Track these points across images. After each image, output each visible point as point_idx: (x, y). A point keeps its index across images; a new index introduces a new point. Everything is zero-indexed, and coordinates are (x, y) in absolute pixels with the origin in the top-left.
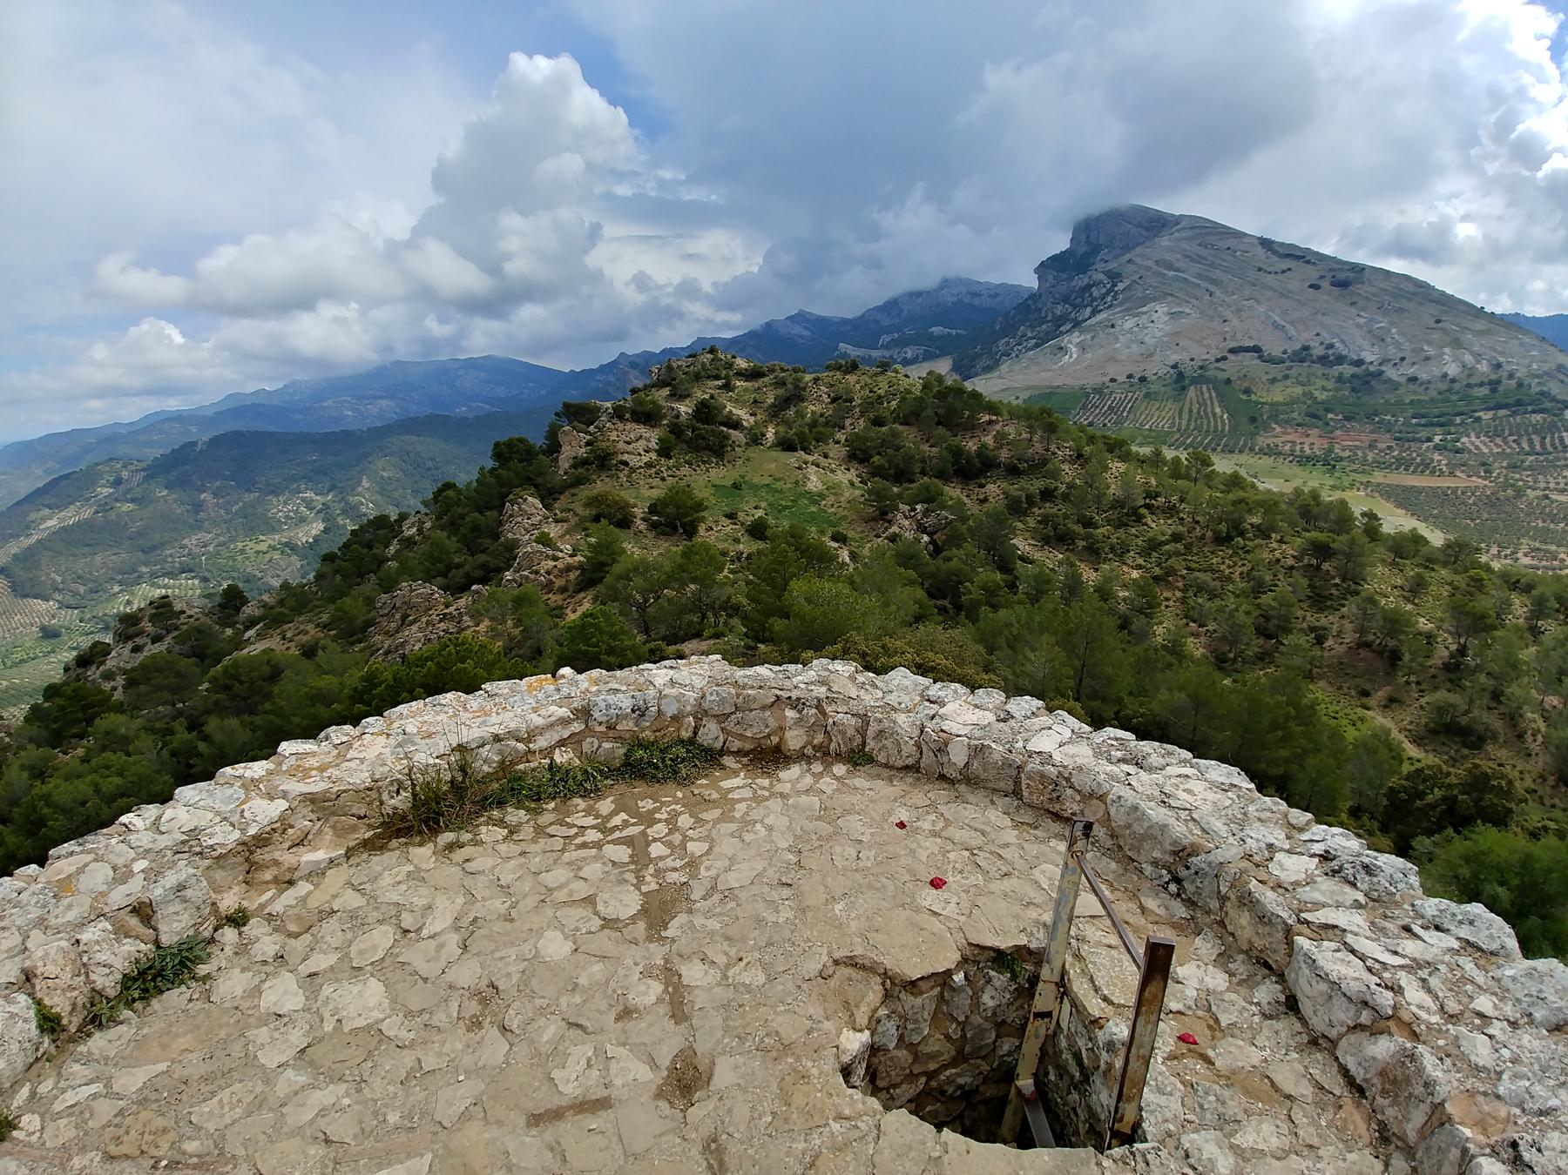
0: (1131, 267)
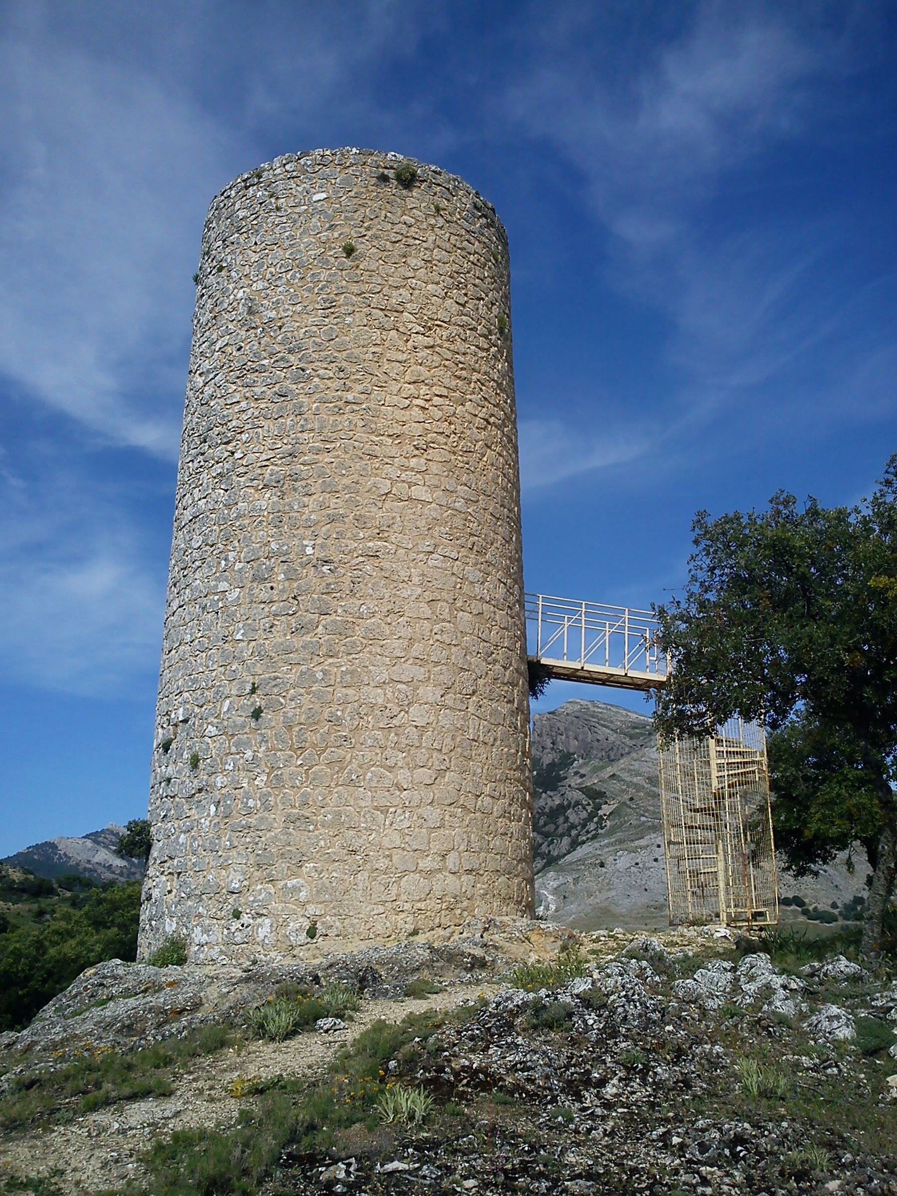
0: (616, 786)
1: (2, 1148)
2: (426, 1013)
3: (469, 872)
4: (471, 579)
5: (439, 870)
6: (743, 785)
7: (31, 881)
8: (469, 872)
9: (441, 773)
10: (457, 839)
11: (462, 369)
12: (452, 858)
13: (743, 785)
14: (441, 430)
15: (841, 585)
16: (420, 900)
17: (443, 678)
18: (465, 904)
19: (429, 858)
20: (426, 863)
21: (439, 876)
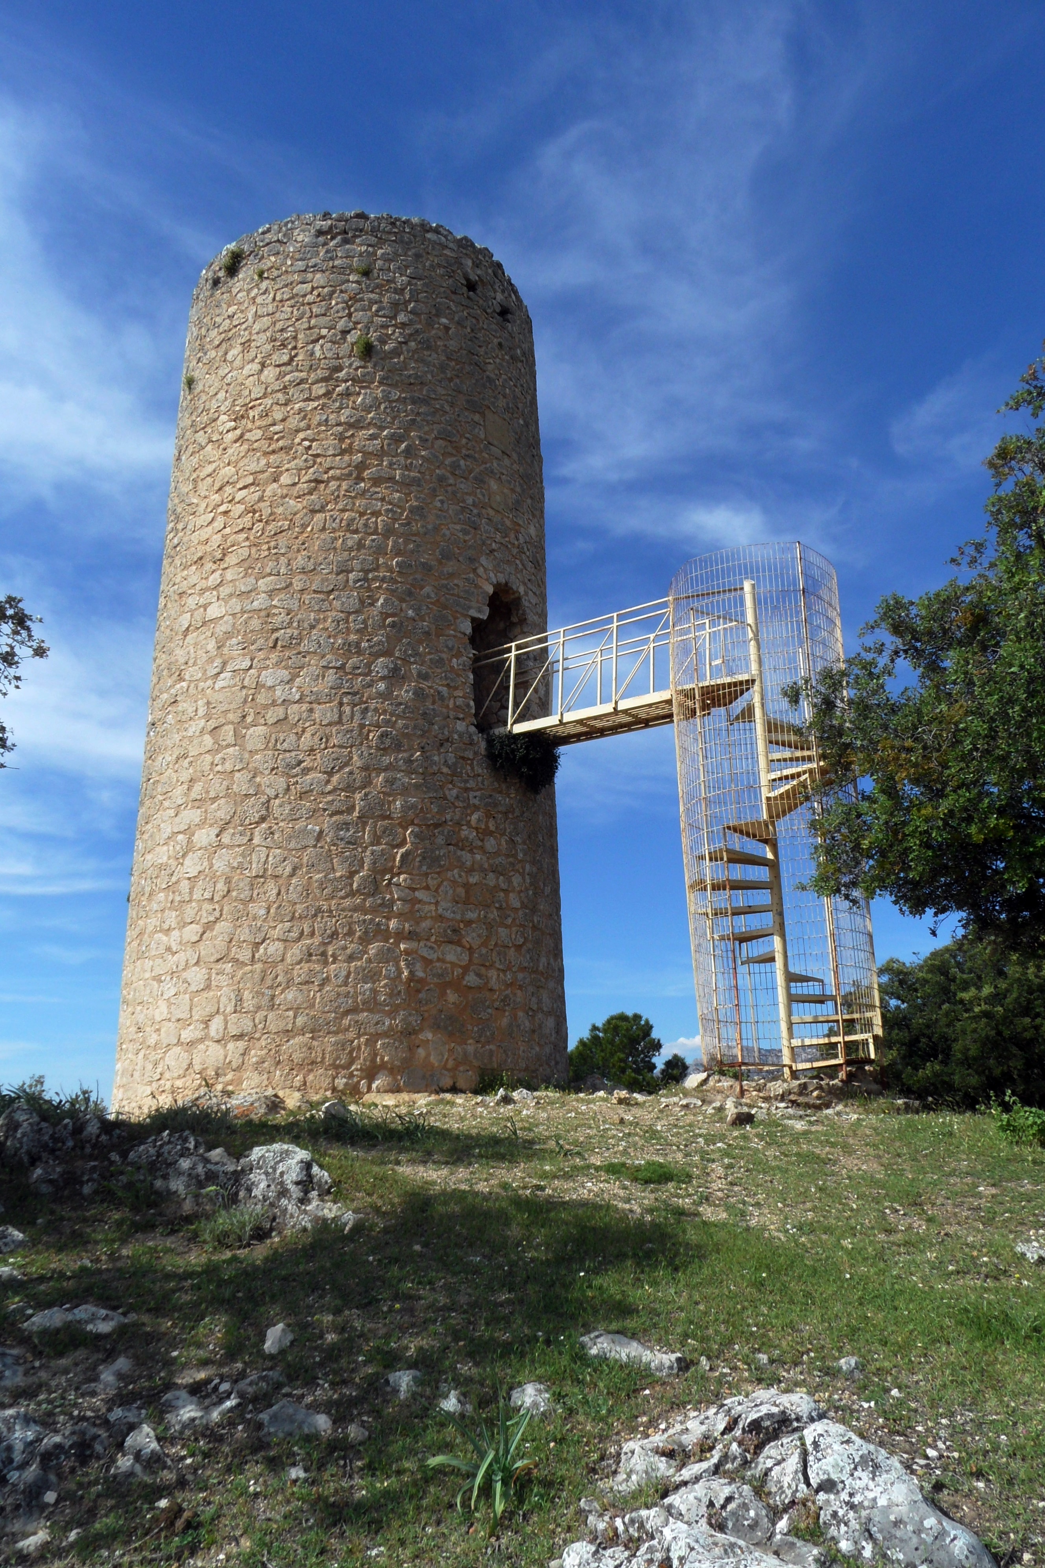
1: (4, 1270)
2: (879, 1094)
3: (240, 1037)
4: (269, 684)
5: (202, 1040)
6: (776, 731)
7: (587, 1329)
8: (240, 1037)
9: (209, 926)
10: (224, 1000)
11: (278, 440)
12: (216, 1025)
13: (776, 731)
14: (241, 527)
15: (389, 919)
16: (179, 1077)
17: (221, 814)
18: (229, 1077)
19: (192, 1027)
20: (187, 1035)
21: (201, 1047)
